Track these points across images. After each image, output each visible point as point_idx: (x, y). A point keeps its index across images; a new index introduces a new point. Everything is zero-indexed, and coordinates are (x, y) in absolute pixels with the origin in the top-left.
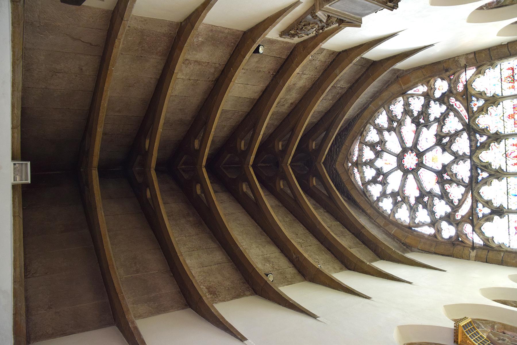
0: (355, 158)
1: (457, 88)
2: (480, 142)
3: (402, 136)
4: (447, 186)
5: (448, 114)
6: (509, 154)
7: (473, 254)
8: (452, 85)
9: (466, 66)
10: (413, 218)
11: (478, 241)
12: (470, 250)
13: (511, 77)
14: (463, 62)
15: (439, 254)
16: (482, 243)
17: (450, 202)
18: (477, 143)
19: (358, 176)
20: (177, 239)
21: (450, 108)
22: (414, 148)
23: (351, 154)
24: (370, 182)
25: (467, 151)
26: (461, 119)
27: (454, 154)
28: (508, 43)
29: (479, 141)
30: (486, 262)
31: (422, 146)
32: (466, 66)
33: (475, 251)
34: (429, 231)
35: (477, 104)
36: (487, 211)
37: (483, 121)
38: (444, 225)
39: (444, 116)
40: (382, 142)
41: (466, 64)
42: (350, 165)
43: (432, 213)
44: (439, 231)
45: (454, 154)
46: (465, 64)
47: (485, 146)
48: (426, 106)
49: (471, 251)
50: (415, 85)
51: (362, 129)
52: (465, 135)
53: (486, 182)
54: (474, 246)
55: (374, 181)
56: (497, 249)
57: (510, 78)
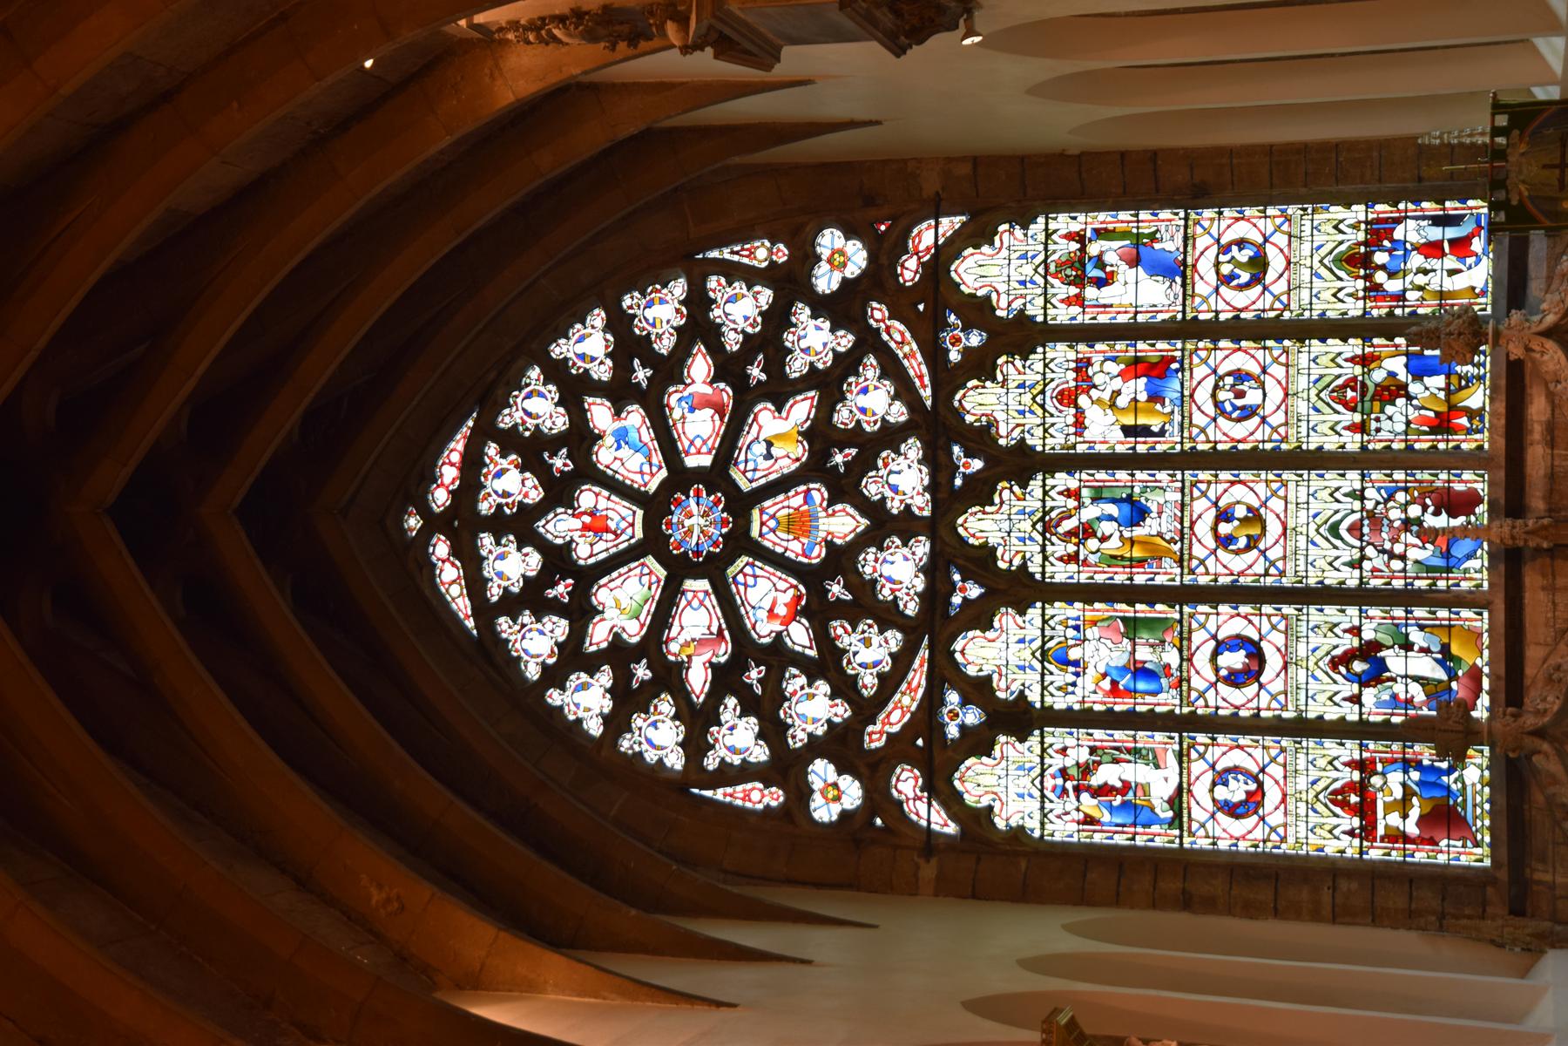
0: (440, 498)
1: (899, 271)
2: (964, 474)
3: (671, 424)
4: (838, 627)
5: (859, 361)
6: (1053, 523)
7: (928, 871)
8: (885, 253)
9: (941, 200)
10: (695, 745)
11: (941, 822)
12: (916, 858)
13: (1077, 265)
14: (931, 184)
15: (804, 884)
16: (952, 829)
17: (844, 687)
18: (954, 478)
19: (449, 573)
21: (869, 341)
22: (717, 477)
23: (430, 477)
24: (511, 605)
25: (921, 504)
26: (904, 390)
27: (867, 507)
28: (1083, 154)
29: (962, 469)
30: (975, 896)
31: (752, 469)
32: (941, 200)
33: (934, 861)
34: (760, 797)
35: (963, 341)
36: (972, 717)
37: (978, 401)
38: (821, 771)
39: (847, 364)
40: (581, 438)
41: (941, 192)
42: (414, 523)
43: (773, 731)
44: (800, 794)
45: (867, 507)
46: (937, 193)
47: (980, 492)
48: (777, 319)
49: (921, 861)
50: (744, 234)
51: (492, 376)
52: (913, 449)
53: (980, 617)
54: (933, 842)
55: (532, 599)
56: (1008, 848)
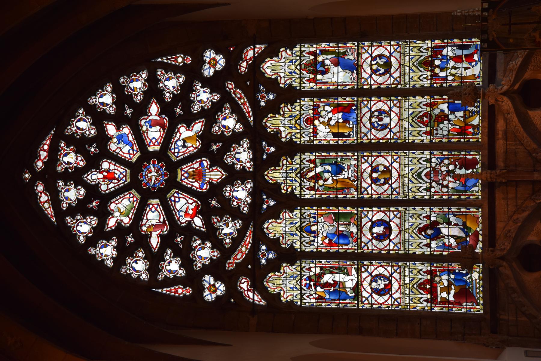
5: (222, 106)
17: (217, 244)
20: (355, 183)
21: (226, 98)
38: (208, 280)
39: (217, 107)
44: (199, 289)
57: (311, 66)
